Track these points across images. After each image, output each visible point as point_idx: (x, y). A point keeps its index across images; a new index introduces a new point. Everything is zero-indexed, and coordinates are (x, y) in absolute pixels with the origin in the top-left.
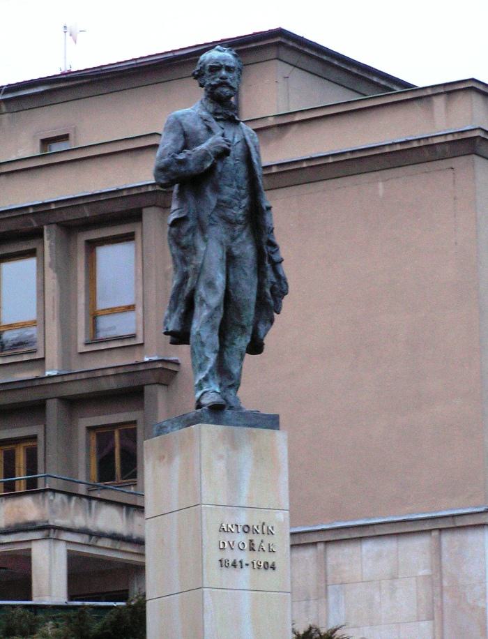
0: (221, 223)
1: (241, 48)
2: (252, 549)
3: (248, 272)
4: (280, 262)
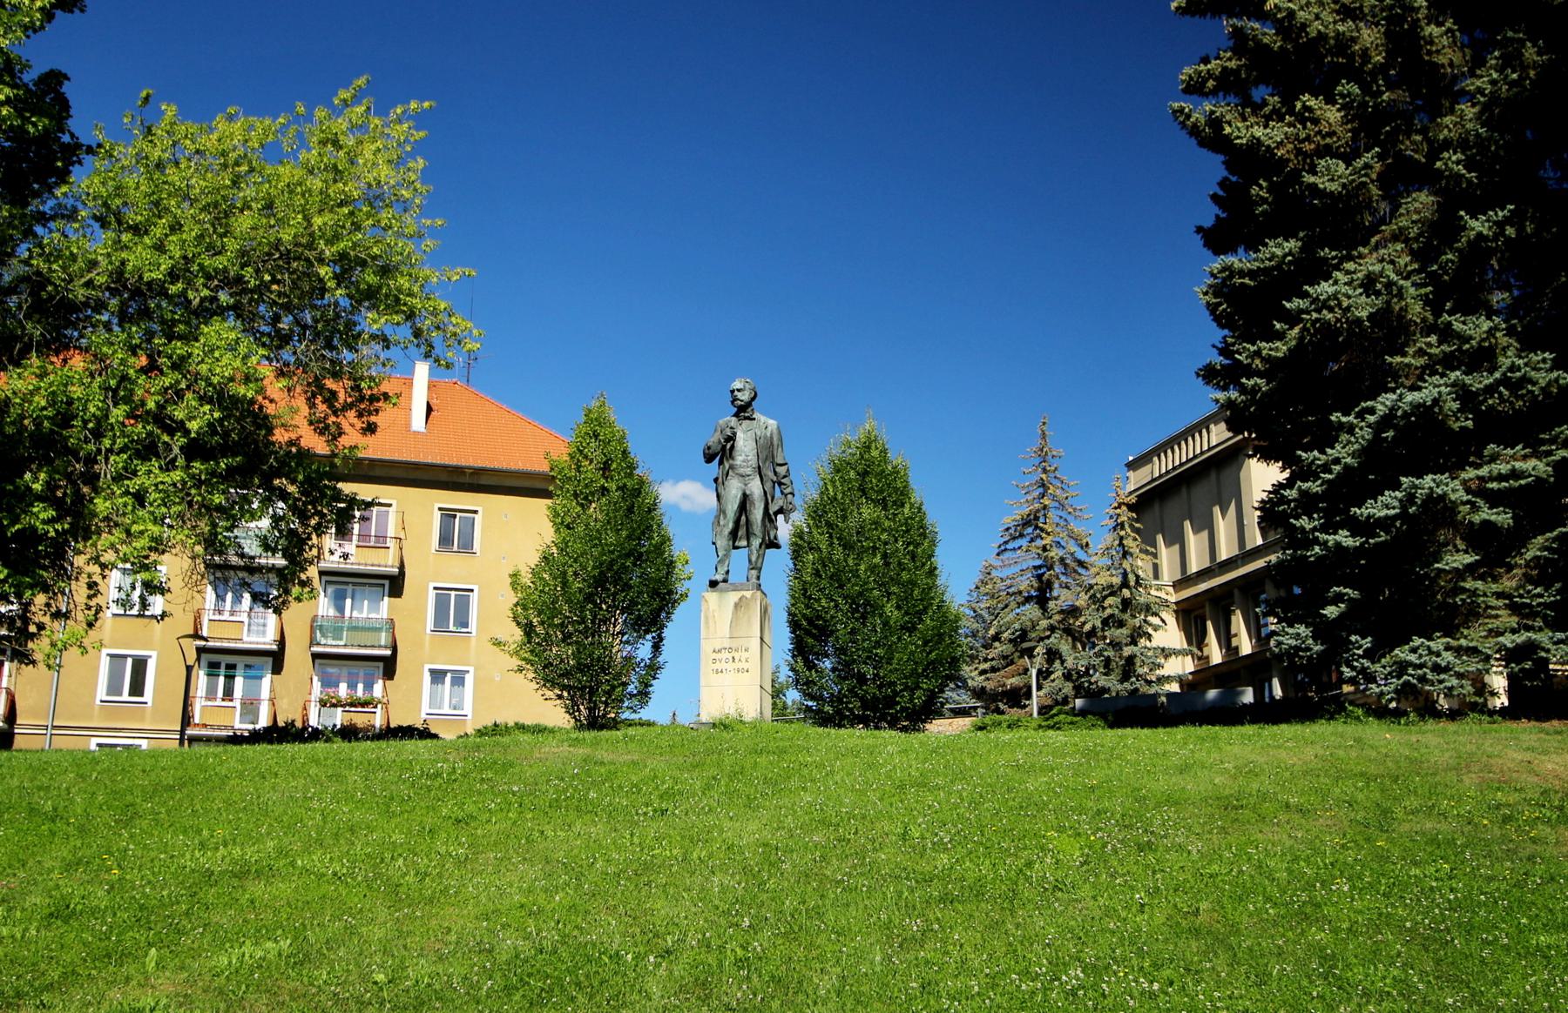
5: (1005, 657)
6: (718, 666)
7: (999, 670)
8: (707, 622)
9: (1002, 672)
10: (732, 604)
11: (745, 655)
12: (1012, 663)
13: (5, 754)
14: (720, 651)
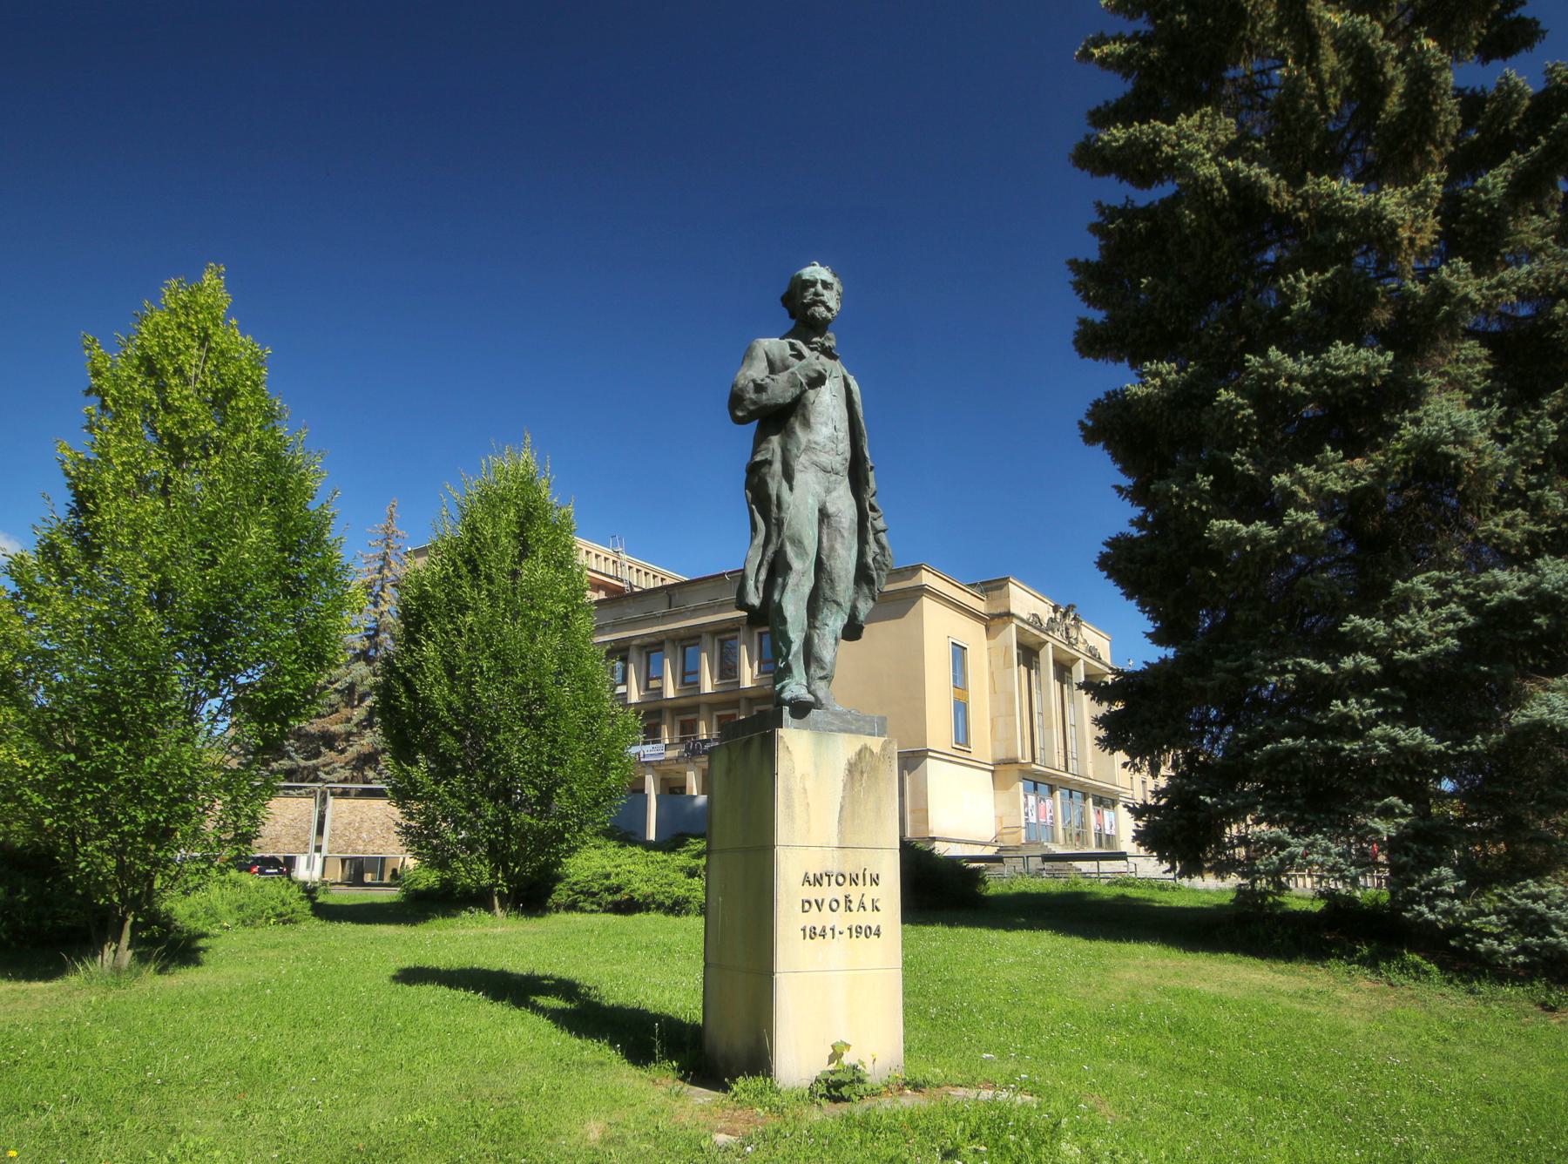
3: (846, 534)
4: (987, 629)
5: (331, 706)
6: (814, 918)
7: (324, 716)
8: (789, 806)
9: (327, 719)
10: (842, 766)
11: (871, 892)
12: (337, 711)
13: (1322, 3)
14: (818, 881)
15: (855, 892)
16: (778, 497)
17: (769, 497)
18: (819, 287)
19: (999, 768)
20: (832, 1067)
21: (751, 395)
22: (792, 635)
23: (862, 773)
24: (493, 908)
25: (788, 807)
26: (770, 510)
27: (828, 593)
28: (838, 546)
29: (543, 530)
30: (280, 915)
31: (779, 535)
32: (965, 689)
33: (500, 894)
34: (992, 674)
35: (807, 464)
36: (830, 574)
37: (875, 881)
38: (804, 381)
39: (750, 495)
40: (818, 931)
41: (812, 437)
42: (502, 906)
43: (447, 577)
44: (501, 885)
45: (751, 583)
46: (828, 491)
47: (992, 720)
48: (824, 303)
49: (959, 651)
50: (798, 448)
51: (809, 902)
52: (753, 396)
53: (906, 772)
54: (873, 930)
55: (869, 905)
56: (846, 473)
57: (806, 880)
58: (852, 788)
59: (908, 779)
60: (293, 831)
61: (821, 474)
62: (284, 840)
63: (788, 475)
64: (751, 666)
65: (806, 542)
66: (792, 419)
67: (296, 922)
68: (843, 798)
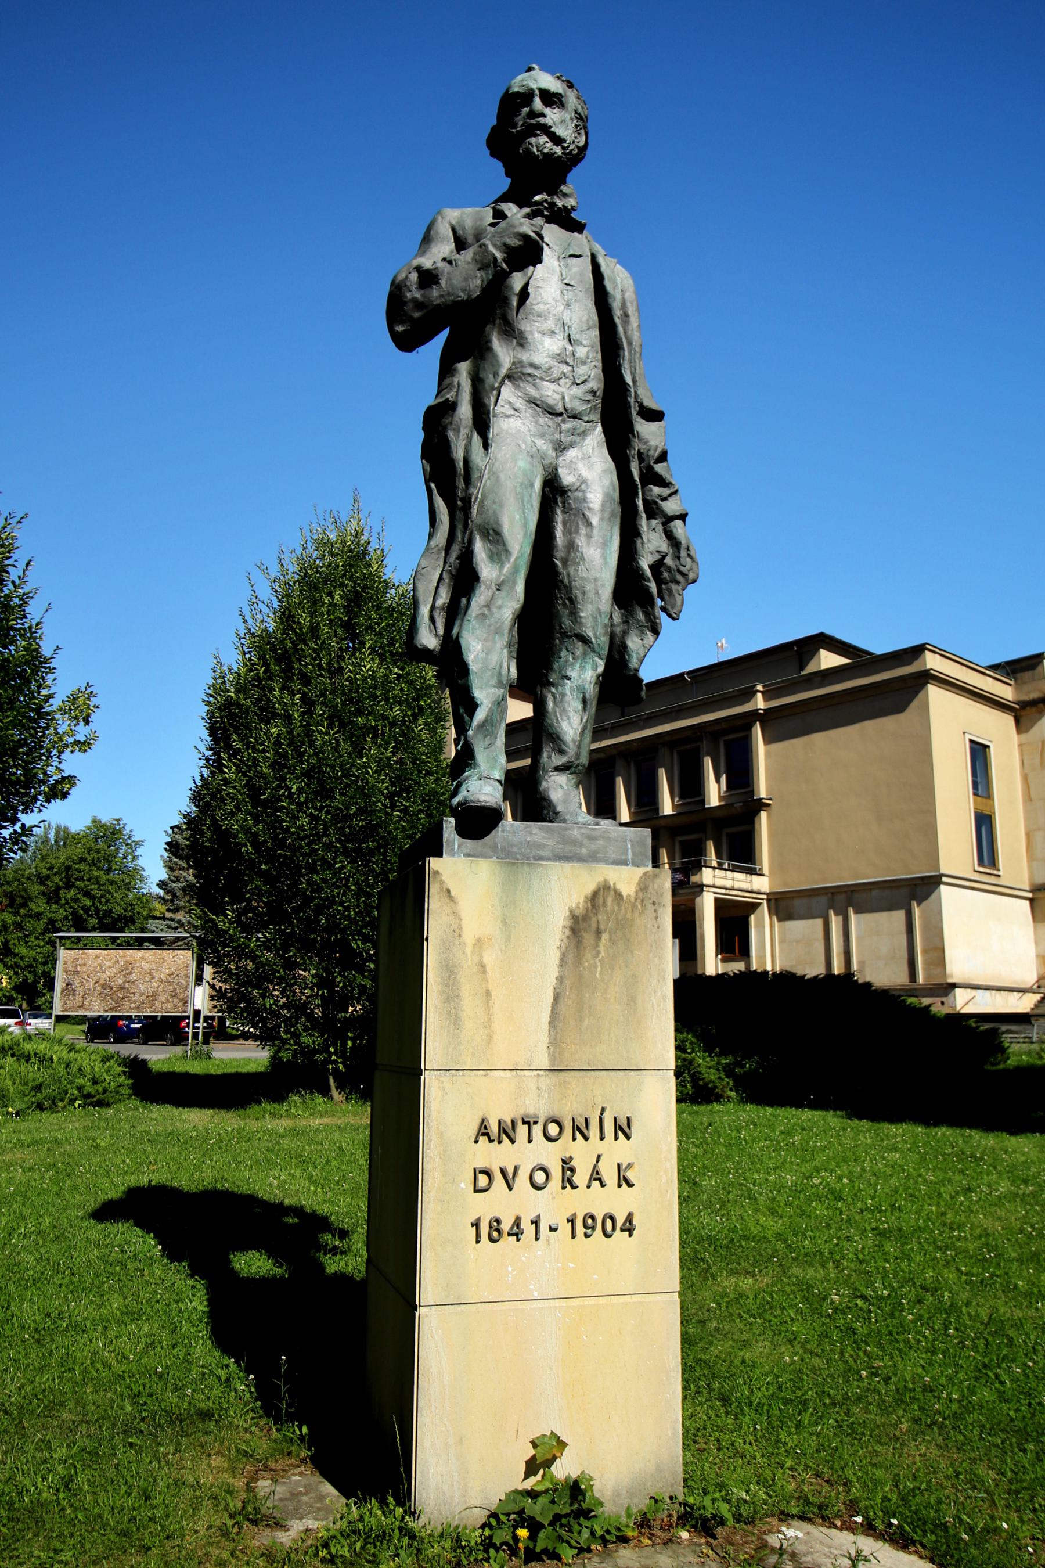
0: (527, 412)
1: (731, 737)
2: (568, 1182)
3: (595, 520)
4: (1017, 721)
8: (451, 996)
14: (506, 1132)
15: (582, 1154)
16: (466, 461)
17: (452, 462)
18: (538, 104)
19: (1039, 895)
20: (530, 1483)
21: (414, 293)
22: (478, 694)
23: (598, 932)
24: (329, 1090)
25: (448, 999)
26: (455, 488)
27: (567, 623)
28: (581, 541)
29: (373, 615)
30: (89, 1096)
31: (466, 526)
32: (989, 796)
33: (336, 1073)
34: (1025, 778)
35: (520, 404)
36: (569, 589)
37: (623, 1129)
38: (499, 256)
39: (428, 468)
40: (506, 1226)
41: (525, 356)
42: (340, 1088)
43: (257, 678)
44: (335, 1062)
45: (424, 610)
46: (561, 448)
47: (1028, 835)
48: (546, 130)
49: (979, 752)
50: (496, 374)
51: (487, 1173)
52: (418, 295)
53: (914, 904)
54: (620, 1222)
55: (610, 1175)
56: (596, 417)
57: (483, 1131)
58: (579, 960)
59: (917, 912)
60: (171, 988)
61: (545, 420)
62: (162, 998)
63: (482, 423)
64: (718, 781)
65: (506, 530)
66: (488, 327)
67: (108, 1105)
68: (560, 979)
